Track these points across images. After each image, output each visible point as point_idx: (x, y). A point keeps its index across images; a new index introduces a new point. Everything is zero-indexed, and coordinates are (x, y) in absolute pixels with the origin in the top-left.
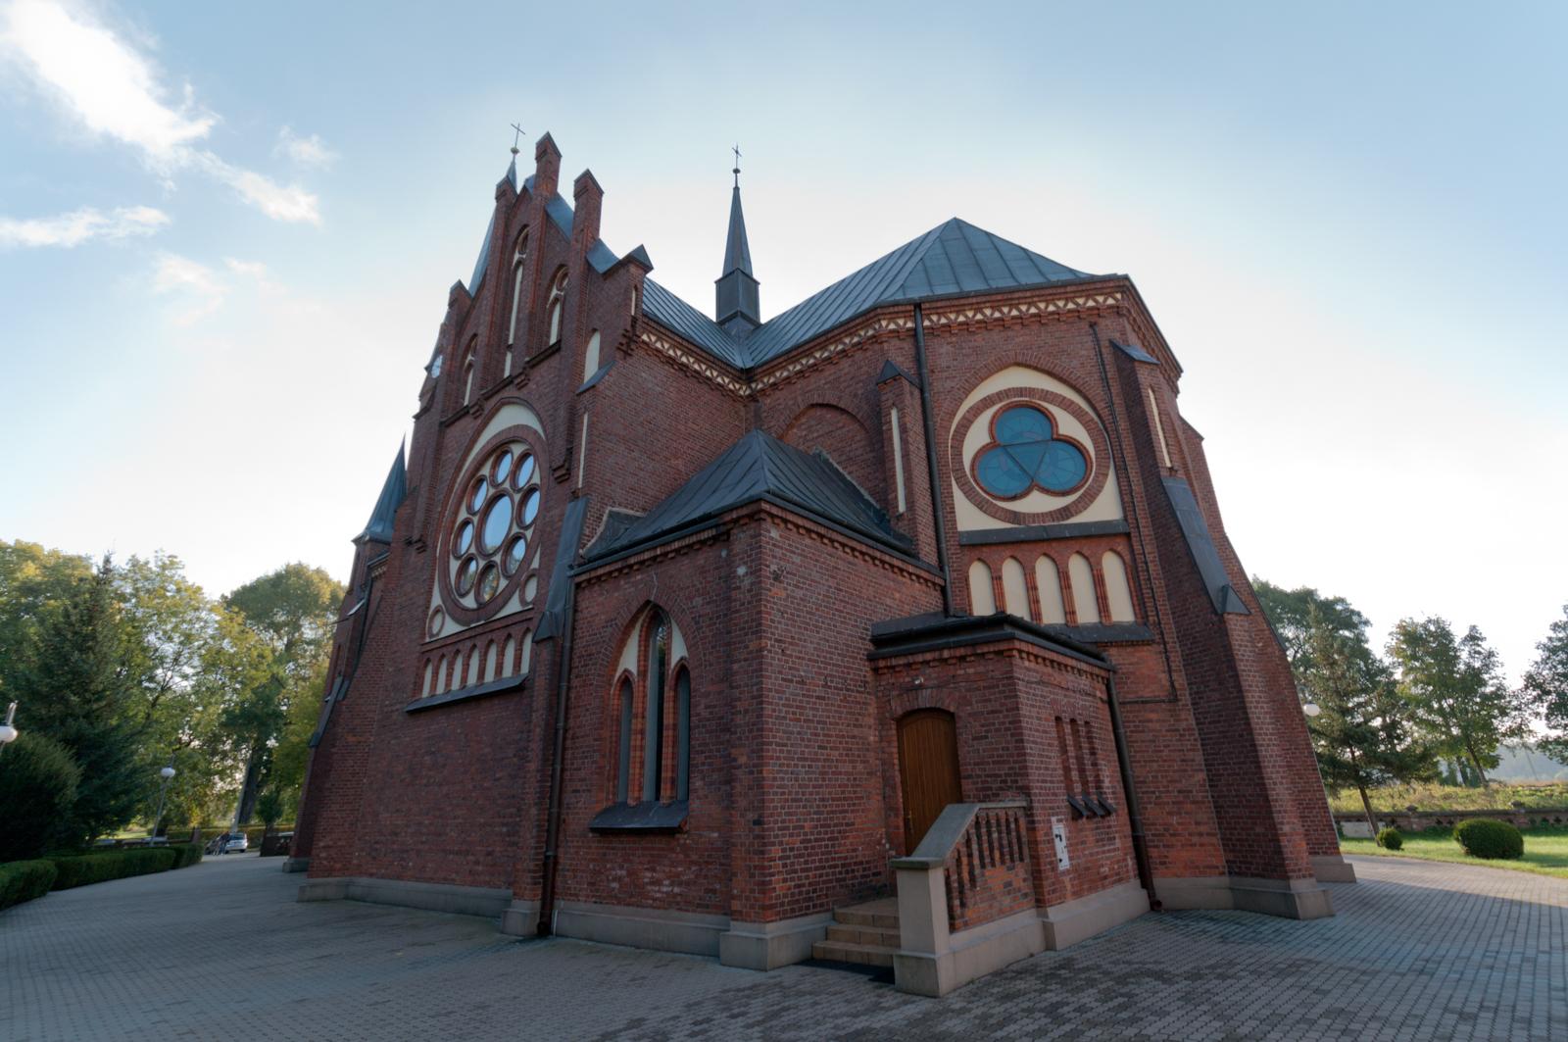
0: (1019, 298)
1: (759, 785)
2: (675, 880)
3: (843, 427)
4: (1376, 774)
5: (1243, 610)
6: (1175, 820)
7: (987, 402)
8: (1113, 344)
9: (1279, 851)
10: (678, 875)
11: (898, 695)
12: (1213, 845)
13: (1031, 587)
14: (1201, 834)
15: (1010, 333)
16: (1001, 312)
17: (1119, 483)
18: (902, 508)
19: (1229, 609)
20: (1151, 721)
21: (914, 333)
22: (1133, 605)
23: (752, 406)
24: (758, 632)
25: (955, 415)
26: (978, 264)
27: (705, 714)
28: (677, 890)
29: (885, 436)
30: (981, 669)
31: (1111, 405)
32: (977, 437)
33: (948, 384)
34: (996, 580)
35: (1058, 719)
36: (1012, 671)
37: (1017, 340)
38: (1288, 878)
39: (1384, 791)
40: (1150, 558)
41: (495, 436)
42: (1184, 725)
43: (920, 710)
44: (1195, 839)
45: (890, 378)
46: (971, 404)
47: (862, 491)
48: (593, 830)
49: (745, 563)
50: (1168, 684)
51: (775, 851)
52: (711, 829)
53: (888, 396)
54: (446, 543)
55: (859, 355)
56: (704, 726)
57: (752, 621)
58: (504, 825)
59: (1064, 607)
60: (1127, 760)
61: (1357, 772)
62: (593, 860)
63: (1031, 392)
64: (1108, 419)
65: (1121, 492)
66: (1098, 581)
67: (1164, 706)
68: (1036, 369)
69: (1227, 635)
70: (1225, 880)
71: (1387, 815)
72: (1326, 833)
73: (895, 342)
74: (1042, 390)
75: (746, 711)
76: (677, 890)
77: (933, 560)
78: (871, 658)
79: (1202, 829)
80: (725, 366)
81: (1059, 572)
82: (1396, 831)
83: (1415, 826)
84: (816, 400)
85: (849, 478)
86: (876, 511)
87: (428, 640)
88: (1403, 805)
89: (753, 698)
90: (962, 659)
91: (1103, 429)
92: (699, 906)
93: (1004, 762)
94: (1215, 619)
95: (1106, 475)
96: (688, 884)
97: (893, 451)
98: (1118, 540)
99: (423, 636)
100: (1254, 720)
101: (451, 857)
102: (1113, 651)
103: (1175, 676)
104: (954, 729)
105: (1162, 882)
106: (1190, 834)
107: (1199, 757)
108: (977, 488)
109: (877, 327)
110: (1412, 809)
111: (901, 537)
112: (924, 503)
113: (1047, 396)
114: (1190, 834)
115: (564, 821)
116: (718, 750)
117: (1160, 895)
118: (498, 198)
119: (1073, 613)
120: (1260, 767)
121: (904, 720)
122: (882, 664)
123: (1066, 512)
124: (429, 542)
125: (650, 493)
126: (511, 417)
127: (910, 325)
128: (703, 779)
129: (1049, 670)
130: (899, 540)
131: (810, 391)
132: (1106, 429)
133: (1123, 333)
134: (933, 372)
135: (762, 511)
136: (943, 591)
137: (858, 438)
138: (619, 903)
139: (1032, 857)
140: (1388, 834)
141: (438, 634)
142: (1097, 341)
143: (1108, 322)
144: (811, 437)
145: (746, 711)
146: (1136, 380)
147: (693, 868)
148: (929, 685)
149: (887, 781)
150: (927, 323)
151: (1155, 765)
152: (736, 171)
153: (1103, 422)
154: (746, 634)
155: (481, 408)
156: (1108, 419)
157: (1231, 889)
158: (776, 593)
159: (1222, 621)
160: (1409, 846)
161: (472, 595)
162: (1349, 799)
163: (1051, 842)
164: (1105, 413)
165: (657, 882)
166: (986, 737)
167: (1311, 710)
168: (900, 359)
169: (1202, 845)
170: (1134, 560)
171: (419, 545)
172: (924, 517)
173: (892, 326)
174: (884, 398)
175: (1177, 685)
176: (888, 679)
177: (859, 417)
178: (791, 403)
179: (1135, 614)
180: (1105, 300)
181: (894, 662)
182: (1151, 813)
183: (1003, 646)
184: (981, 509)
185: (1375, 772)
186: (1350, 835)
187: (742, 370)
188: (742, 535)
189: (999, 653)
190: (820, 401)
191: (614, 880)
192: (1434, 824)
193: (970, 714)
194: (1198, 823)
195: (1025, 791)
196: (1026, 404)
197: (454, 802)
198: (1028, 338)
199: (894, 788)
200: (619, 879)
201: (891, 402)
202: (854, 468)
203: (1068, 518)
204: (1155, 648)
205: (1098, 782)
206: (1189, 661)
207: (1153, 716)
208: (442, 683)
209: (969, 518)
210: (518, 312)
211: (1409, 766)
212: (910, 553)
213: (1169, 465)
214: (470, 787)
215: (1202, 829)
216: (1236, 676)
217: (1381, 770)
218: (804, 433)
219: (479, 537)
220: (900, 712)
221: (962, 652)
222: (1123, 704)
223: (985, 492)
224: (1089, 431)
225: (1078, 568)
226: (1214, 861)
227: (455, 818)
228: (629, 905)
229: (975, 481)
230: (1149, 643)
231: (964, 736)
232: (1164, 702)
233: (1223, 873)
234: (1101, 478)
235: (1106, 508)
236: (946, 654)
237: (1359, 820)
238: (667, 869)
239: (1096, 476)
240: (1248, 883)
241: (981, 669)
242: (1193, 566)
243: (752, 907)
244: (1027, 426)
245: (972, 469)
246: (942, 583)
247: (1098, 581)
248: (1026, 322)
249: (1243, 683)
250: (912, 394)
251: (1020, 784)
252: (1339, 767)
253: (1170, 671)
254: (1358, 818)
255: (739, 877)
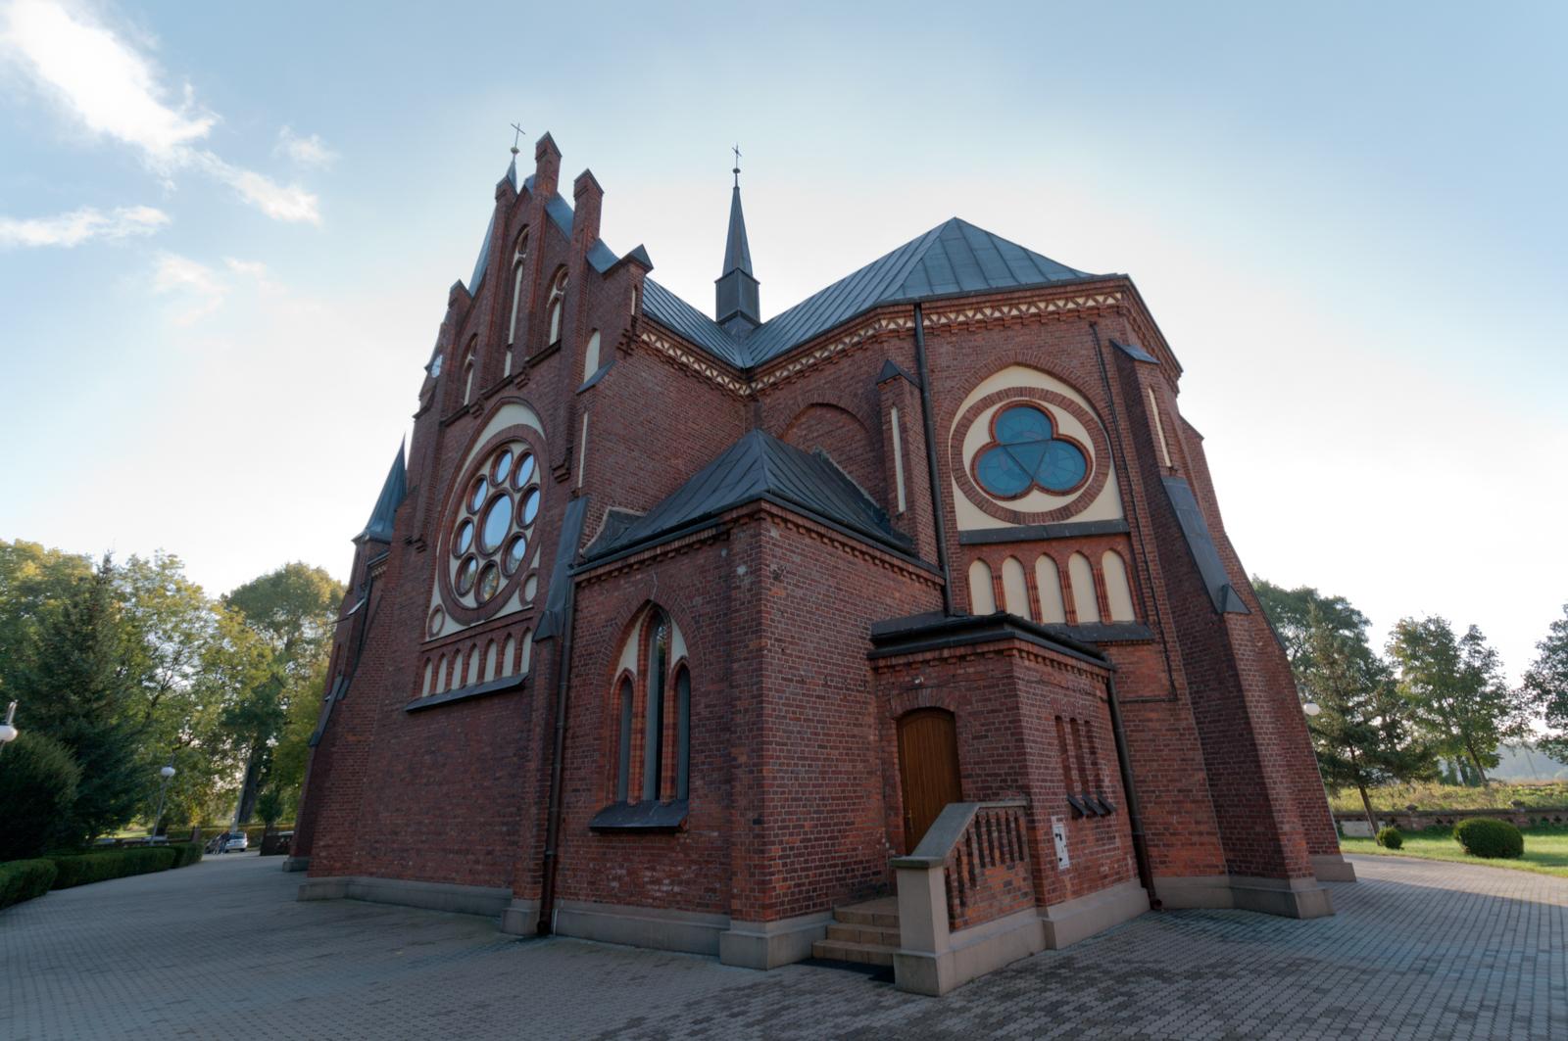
0: (1019, 298)
1: (759, 784)
2: (675, 879)
3: (843, 427)
4: (1376, 773)
5: (1243, 610)
6: (1175, 819)
7: (987, 402)
8: (1113, 344)
9: (1279, 850)
10: (678, 874)
11: (898, 695)
12: (1213, 844)
13: (1031, 587)
14: (1201, 834)
15: (1010, 333)
16: (1001, 311)
17: (1119, 483)
18: (902, 507)
19: (1229, 609)
20: (1151, 720)
21: (914, 333)
22: (1133, 605)
23: (752, 405)
24: (758, 632)
25: (955, 415)
26: (978, 264)
27: (705, 713)
28: (677, 889)
29: (885, 435)
30: (981, 668)
31: (1111, 404)
32: (977, 437)
33: (948, 384)
34: (996, 579)
35: (1058, 718)
36: (1012, 671)
37: (1017, 340)
38: (1288, 877)
39: (1384, 790)
40: (1150, 557)
41: (495, 436)
42: (1184, 724)
43: (920, 710)
44: (1195, 838)
45: (890, 377)
46: (971, 404)
47: (862, 490)
48: (593, 829)
49: (745, 563)
50: (1168, 683)
51: (775, 850)
52: (711, 828)
53: (888, 396)
54: (446, 543)
55: (859, 355)
56: (704, 725)
57: (752, 620)
58: (504, 824)
59: (1064, 606)
60: (1127, 760)
61: (1357, 771)
62: (593, 859)
63: (1031, 391)
64: (1108, 418)
65: (1121, 491)
66: (1098, 581)
67: (1164, 705)
68: (1036, 368)
69: (1227, 634)
70: (1225, 879)
71: (1387, 814)
72: (1326, 833)
73: (895, 341)
74: (1042, 390)
75: (746, 711)
76: (677, 889)
77: (933, 559)
78: (871, 657)
79: (1202, 828)
80: (725, 366)
81: (1059, 572)
82: (1396, 830)
83: (1415, 825)
84: (816, 399)
85: (849, 477)
86: (876, 511)
87: (428, 639)
88: (1403, 804)
89: (753, 697)
90: (962, 658)
91: (1103, 428)
92: (699, 905)
93: (1004, 761)
94: (1215, 618)
95: (1106, 475)
96: (688, 883)
97: (893, 450)
98: (1118, 539)
99: (423, 635)
100: (1254, 720)
101: (451, 856)
102: (1113, 651)
103: (1175, 675)
104: (954, 728)
105: (1162, 882)
106: (1190, 834)
107: (1199, 756)
108: (977, 488)
109: (877, 326)
110: (1412, 808)
111: (901, 537)
112: (924, 502)
113: (1047, 395)
114: (1190, 834)
115: (564, 820)
116: (718, 750)
117: (1160, 894)
118: (498, 198)
119: (1073, 612)
120: (1260, 767)
121: (904, 719)
122: (882, 663)
123: (1066, 512)
124: (429, 541)
125: (650, 492)
126: (511, 417)
127: (910, 324)
128: (703, 778)
129: (1049, 669)
130: (899, 539)
131: (810, 391)
132: (1106, 428)
133: (1123, 333)
134: (933, 371)
135: (762, 510)
136: (943, 590)
137: (858, 438)
138: (619, 902)
139: (1032, 856)
140: (1388, 833)
141: (438, 633)
142: (1097, 340)
143: (1108, 322)
144: (811, 436)
145: (746, 711)
146: (1136, 380)
147: (693, 868)
148: (929, 684)
149: (887, 780)
150: (927, 323)
151: (1155, 764)
152: (736, 171)
153: (1103, 421)
154: (746, 634)
155: (481, 408)
156: (1108, 418)
157: (1231, 888)
158: (776, 592)
159: (1222, 620)
160: (1409, 845)
161: (472, 595)
162: (1349, 799)
163: (1051, 841)
164: (1105, 412)
165: (657, 882)
166: (986, 737)
167: (1311, 709)
168: (900, 359)
169: (1202, 844)
170: (1134, 559)
171: (419, 544)
172: (924, 517)
173: (892, 326)
174: (884, 398)
175: (1177, 684)
176: (888, 678)
177: (859, 417)
178: (791, 402)
179: (1135, 613)
180: (1105, 300)
181: (894, 661)
182: (1151, 812)
183: (1003, 646)
184: (981, 508)
185: (1375, 771)
186: (1350, 834)
187: (742, 370)
188: (742, 535)
189: (999, 652)
190: (820, 401)
191: (614, 879)
192: (1434, 823)
193: (970, 714)
194: (1198, 823)
195: (1025, 790)
196: (1026, 404)
197: (454, 801)
198: (1028, 338)
199: (894, 787)
200: (619, 878)
201: (891, 401)
202: (854, 467)
203: (1068, 518)
204: (1155, 647)
205: (1098, 781)
206: (1189, 660)
207: (1153, 715)
208: (442, 682)
209: (969, 518)
210: (518, 312)
211: (1409, 766)
212: (910, 553)
213: (1169, 464)
214: (470, 786)
215: (1202, 828)
216: (1236, 676)
217: (1381, 770)
218: (804, 433)
219: (479, 536)
220: (900, 711)
221: (962, 651)
222: (1123, 703)
223: (985, 491)
224: (1089, 430)
225: (1078, 568)
226: (1214, 860)
227: (455, 817)
228: (629, 904)
229: (975, 480)
230: (1149, 642)
231: (964, 735)
232: (1164, 701)
233: (1223, 873)
234: (1101, 478)
235: (1106, 507)
236: (946, 653)
237: (1359, 820)
238: (667, 869)
239: (1096, 475)
240: (1248, 882)
241: (981, 668)
242: (1193, 565)
243: (752, 906)
244: (1027, 426)
245: (972, 468)
246: (942, 582)
247: (1098, 581)
248: (1026, 322)
249: (1243, 683)
250: (912, 393)
251: (1020, 783)
252: (1339, 767)
253: (1170, 671)
254: (1358, 817)
255: (739, 877)
